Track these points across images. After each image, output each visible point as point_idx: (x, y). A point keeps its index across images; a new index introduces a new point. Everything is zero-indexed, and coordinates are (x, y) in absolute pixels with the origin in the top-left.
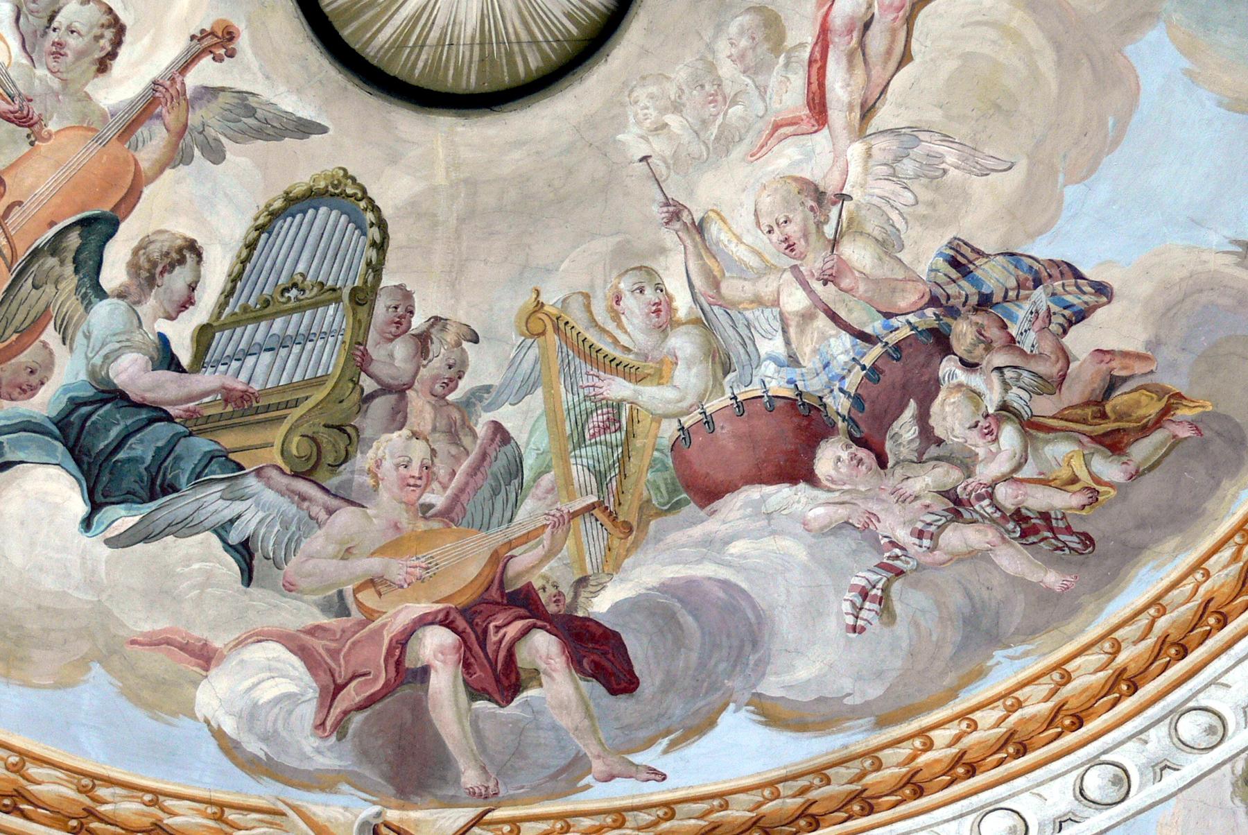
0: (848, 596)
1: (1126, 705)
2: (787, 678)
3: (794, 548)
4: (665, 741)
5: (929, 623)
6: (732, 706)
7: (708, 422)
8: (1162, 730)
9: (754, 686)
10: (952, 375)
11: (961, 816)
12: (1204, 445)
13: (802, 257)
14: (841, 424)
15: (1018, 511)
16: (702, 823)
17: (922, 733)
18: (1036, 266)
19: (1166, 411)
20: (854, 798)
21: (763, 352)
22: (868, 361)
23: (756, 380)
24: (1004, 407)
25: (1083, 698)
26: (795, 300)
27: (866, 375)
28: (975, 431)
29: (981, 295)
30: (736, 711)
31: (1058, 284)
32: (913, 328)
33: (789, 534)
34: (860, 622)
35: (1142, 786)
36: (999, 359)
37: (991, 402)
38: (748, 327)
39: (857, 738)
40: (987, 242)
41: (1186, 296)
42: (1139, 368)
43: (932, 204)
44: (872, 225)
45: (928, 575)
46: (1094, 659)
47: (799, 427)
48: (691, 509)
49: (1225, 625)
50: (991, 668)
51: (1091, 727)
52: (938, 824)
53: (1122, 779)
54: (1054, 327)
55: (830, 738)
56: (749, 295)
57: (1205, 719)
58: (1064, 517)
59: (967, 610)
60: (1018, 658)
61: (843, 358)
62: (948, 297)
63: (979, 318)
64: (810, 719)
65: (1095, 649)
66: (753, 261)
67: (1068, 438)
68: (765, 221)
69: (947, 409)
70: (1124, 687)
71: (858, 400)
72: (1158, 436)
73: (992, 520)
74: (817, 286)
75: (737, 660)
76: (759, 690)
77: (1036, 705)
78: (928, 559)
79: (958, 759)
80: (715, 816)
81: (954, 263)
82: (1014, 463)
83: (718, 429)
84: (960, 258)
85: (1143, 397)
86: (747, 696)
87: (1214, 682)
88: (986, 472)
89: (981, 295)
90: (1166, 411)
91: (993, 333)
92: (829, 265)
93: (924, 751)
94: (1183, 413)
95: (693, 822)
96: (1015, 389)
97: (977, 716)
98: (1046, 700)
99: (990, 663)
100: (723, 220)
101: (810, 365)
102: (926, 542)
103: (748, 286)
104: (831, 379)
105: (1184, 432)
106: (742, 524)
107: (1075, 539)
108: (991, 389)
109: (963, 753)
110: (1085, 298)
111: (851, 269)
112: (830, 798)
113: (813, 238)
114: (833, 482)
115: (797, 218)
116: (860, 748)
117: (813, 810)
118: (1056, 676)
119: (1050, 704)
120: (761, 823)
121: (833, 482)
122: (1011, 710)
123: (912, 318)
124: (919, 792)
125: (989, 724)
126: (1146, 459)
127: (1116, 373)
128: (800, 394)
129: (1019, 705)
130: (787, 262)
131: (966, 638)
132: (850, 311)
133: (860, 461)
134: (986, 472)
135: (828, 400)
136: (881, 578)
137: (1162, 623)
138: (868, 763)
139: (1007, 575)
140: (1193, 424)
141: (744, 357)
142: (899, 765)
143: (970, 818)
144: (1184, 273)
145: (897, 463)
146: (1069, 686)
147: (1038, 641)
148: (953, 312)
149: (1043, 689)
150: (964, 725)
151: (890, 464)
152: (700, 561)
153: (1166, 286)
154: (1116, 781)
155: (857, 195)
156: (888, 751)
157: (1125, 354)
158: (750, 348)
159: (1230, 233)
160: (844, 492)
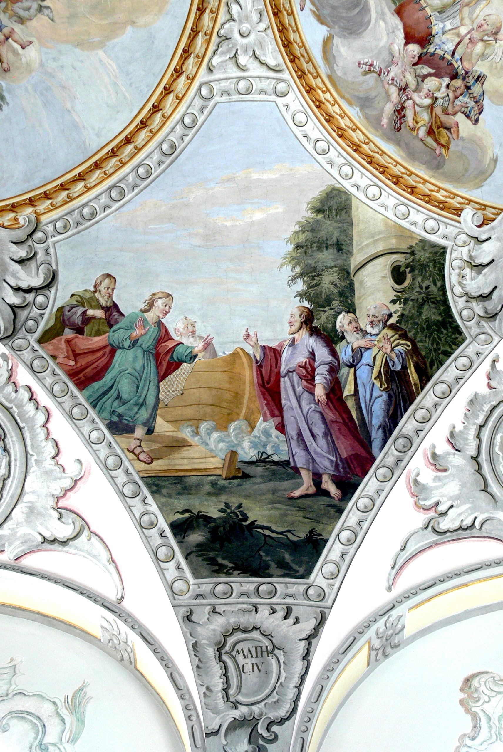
0: (370, 60)
1: (349, 150)
2: (340, 45)
3: (384, 41)
4: (314, 9)
5: (365, 86)
6: (329, 29)
7: (423, 9)
8: (344, 161)
9: (336, 35)
10: (444, 82)
11: (302, 106)
12: (435, 158)
13: (477, 31)
14: (425, 50)
15: (405, 108)
16: (287, 25)
17: (328, 90)
18: (481, 101)
19: (443, 146)
20: (303, 72)
21: (446, 23)
22: (446, 56)
23: (437, 22)
24: (436, 99)
25: (349, 136)
26: (463, 31)
27: (441, 56)
28: (428, 91)
29: (470, 86)
30: (327, 31)
31: (476, 108)
32: (458, 68)
33: (388, 39)
34: (362, 65)
35: (324, 158)
36: (451, 95)
37: (437, 94)
38: (454, 17)
39: (323, 70)
40: (487, 86)
41: (479, 146)
42: (455, 136)
43: (496, 68)
44: (488, 51)
45: (380, 84)
46: (362, 138)
47: (423, 38)
48: (394, 7)
49: (381, 174)
50: (353, 107)
51: (340, 140)
52: (298, 99)
53: (325, 152)
54: (463, 109)
55: (322, 62)
56: (464, 16)
57: (350, 173)
58: (405, 122)
59: (370, 97)
60: (358, 115)
61: (446, 48)
62: (468, 77)
63: (463, 87)
64: (327, 54)
65: (365, 137)
66: (475, 16)
67: (430, 119)
68: (487, 18)
69: (434, 82)
70: (355, 148)
71: (433, 54)
72: (435, 145)
73: (400, 100)
74: (468, 37)
75: (345, 29)
76: (335, 37)
77: (343, 123)
78: (385, 83)
79: (321, 102)
80: (290, 29)
81: (479, 77)
82: (419, 104)
83: (420, 12)
84: (480, 79)
85: (446, 138)
86: (333, 33)
87: (362, 174)
88: (415, 96)
89: (470, 86)
90: (443, 146)
91: (459, 92)
92: (475, 39)
93: (322, 91)
94: (443, 151)
95: (287, 22)
96: (442, 101)
97: (336, 105)
98: (346, 126)
99: (355, 107)
100: (487, 5)
101: (443, 38)
102: (390, 82)
103: (467, 15)
104: (439, 45)
105: (438, 152)
106: (390, 24)
107: (399, 126)
108: (441, 94)
109: (323, 103)
110: (473, 117)
111: (474, 46)
112: (302, 65)
113: (483, 33)
114: (407, 50)
115: (489, 28)
116: (320, 71)
117: (297, 60)
118: (354, 127)
119: (344, 127)
120: (290, 44)
121: (407, 50)
122: (340, 115)
123: (461, 67)
124: (308, 92)
125: (334, 110)
126: (427, 142)
127: (452, 130)
128: (434, 36)
129: (342, 118)
130: (475, 26)
131: (362, 98)
132: (461, 48)
133: (414, 58)
134: (415, 96)
135: (432, 45)
136: (377, 70)
137: (377, 155)
138: (315, 74)
139: (384, 108)
140: (441, 154)
141: (444, 17)
142: (316, 84)
143: (302, 109)
144: (485, 144)
145: (415, 69)
146: (351, 132)
147: (364, 120)
148: (464, 79)
149: (349, 123)
150: (333, 102)
151: (414, 67)
152: (376, 12)
153: (480, 139)
154: (324, 150)
155: (497, 45)
156: (320, 80)
157: (458, 131)
158: (447, 19)
159: (499, 155)
160: (404, 55)
